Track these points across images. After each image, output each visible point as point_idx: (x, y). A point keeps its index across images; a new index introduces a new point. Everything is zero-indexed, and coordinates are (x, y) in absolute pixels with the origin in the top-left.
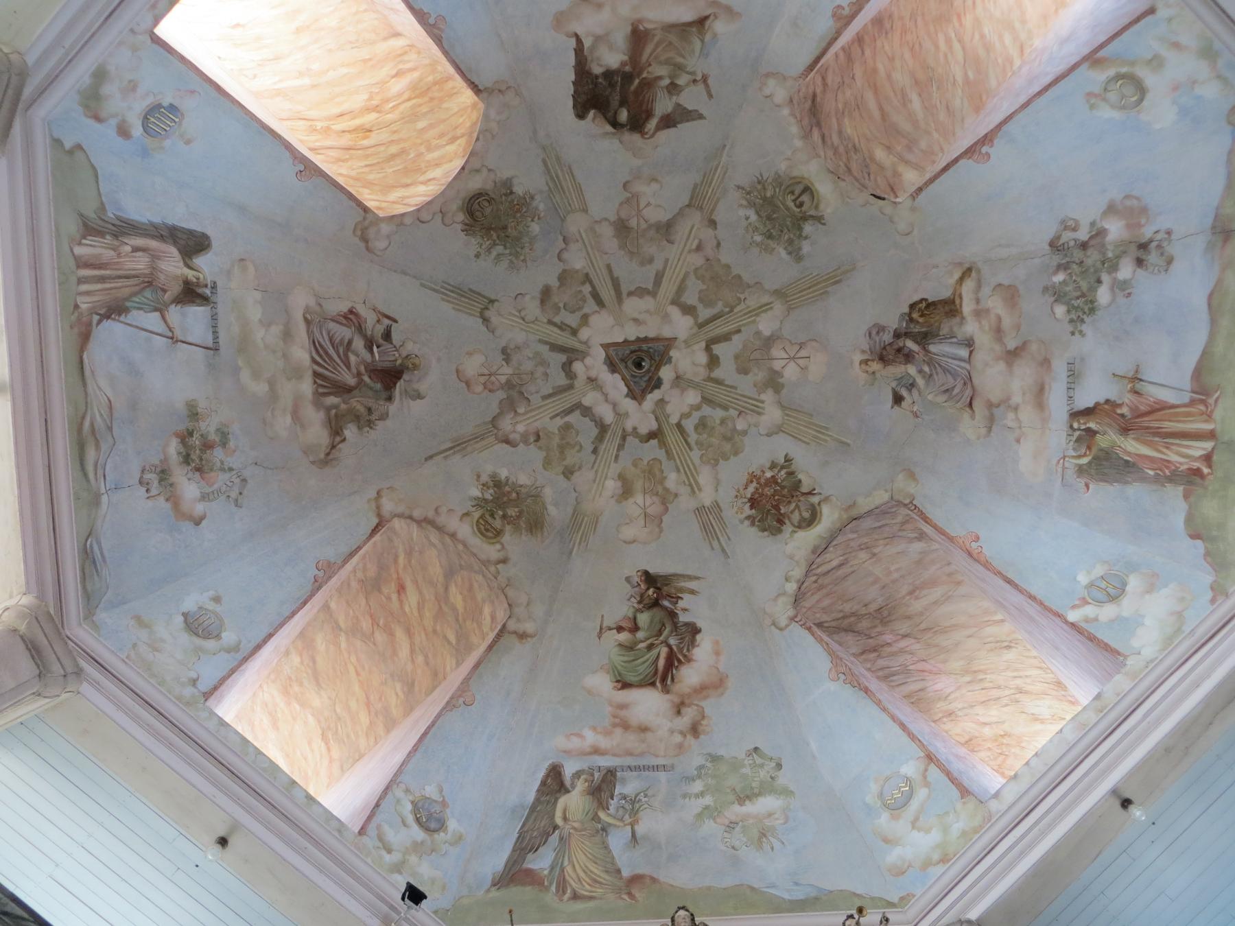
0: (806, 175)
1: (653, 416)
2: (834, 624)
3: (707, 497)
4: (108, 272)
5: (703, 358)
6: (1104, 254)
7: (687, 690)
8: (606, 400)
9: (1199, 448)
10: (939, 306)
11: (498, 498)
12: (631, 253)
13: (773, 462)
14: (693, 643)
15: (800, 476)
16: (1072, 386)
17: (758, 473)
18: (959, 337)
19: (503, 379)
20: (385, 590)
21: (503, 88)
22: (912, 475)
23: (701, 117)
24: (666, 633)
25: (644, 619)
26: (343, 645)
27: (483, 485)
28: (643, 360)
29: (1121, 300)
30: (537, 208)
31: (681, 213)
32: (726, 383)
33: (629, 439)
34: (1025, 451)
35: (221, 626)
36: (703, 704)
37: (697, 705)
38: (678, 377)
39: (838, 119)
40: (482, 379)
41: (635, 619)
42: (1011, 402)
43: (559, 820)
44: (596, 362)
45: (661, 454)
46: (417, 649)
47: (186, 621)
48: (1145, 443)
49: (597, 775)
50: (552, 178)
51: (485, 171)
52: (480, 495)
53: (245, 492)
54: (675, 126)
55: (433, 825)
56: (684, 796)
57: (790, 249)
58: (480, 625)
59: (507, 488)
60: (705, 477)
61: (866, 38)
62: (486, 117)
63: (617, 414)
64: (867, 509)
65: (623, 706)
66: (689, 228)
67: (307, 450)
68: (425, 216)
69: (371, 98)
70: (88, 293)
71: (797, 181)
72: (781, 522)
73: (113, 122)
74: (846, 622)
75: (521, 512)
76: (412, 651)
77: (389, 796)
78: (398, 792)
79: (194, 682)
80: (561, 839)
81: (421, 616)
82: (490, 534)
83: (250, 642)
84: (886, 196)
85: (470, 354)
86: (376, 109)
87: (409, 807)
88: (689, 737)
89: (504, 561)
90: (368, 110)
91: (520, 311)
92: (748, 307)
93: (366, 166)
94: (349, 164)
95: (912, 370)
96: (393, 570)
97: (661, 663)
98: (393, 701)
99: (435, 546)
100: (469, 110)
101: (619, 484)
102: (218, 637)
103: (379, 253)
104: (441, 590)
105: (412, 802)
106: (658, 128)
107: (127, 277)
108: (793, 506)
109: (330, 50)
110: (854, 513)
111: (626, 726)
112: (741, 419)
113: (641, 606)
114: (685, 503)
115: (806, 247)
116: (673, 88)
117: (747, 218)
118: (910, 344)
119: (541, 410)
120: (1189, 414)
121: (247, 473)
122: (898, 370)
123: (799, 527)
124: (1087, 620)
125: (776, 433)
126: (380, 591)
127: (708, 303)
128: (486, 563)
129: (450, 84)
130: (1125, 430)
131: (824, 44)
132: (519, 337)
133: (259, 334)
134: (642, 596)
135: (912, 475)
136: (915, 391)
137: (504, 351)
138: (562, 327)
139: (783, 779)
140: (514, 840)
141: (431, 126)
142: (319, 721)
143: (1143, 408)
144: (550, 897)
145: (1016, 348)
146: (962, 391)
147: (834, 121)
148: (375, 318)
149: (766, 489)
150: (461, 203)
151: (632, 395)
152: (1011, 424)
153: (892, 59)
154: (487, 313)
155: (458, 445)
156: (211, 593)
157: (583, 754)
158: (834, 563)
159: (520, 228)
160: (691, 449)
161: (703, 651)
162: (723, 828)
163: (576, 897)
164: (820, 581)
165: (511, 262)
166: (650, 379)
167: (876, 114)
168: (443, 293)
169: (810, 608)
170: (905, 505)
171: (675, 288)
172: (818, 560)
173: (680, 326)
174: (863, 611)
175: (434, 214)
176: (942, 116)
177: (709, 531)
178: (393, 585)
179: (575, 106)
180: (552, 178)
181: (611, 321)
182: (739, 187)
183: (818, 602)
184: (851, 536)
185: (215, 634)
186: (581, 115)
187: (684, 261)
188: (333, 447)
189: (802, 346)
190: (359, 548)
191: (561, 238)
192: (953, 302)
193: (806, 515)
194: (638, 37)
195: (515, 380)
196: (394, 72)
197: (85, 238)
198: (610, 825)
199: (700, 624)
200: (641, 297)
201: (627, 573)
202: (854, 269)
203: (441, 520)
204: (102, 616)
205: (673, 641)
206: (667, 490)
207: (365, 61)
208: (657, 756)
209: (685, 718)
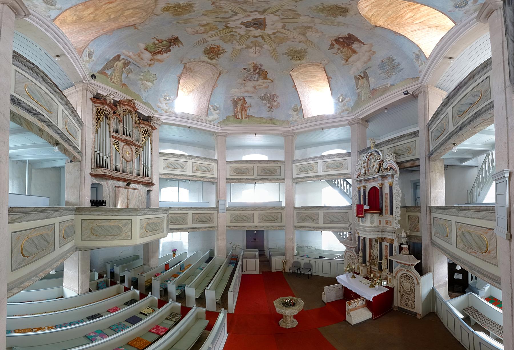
14: (166, 53)
15: (222, 55)
17: (220, 47)
22: (227, 72)
29: (263, 104)
34: (236, 90)
43: (115, 66)
48: (240, 109)
49: (127, 61)
56: (139, 74)
65: (142, 53)
72: (208, 54)
80: (114, 70)
95: (252, 71)
110: (216, 65)
111: (139, 56)
116: (339, 49)
118: (258, 71)
122: (252, 69)
123: (208, 57)
124: (210, 108)
130: (242, 105)
146: (247, 79)
152: (241, 87)
161: (165, 55)
163: (113, 82)
198: (124, 72)
205: (164, 50)
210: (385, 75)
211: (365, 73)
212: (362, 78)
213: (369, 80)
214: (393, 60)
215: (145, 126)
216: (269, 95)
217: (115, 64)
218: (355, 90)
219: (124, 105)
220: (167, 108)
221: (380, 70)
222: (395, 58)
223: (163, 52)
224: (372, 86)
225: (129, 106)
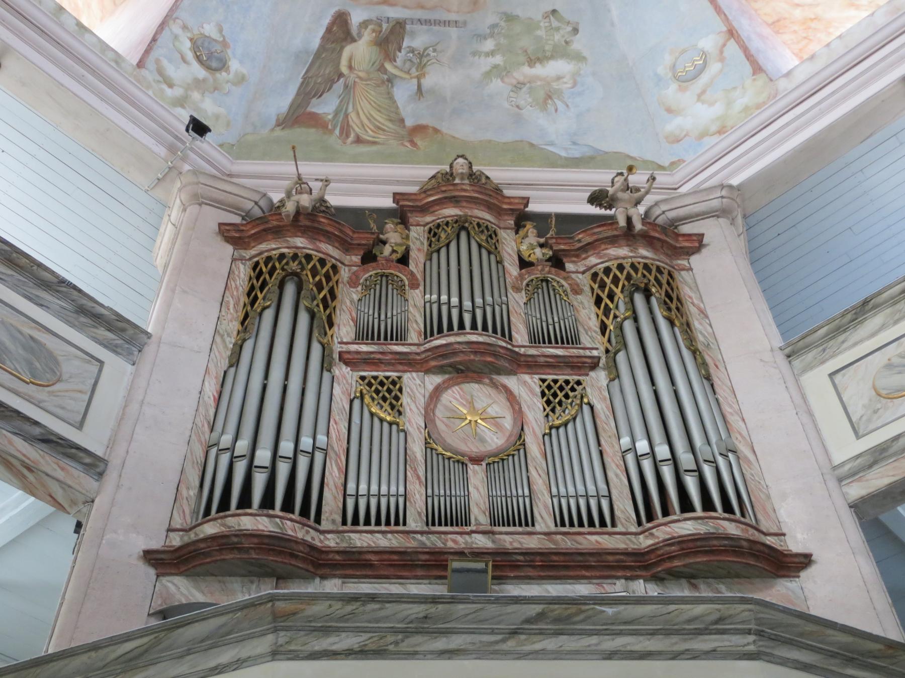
43: (344, 69)
49: (385, 26)
55: (214, 64)
56: (475, 53)
77: (166, 33)
78: (176, 28)
80: (346, 86)
87: (188, 44)
105: (191, 40)
139: (578, 44)
144: (334, 139)
163: (359, 140)
198: (396, 76)
208: (449, 11)
215: (598, 255)
219: (424, 209)
220: (718, 109)
225: (454, 200)
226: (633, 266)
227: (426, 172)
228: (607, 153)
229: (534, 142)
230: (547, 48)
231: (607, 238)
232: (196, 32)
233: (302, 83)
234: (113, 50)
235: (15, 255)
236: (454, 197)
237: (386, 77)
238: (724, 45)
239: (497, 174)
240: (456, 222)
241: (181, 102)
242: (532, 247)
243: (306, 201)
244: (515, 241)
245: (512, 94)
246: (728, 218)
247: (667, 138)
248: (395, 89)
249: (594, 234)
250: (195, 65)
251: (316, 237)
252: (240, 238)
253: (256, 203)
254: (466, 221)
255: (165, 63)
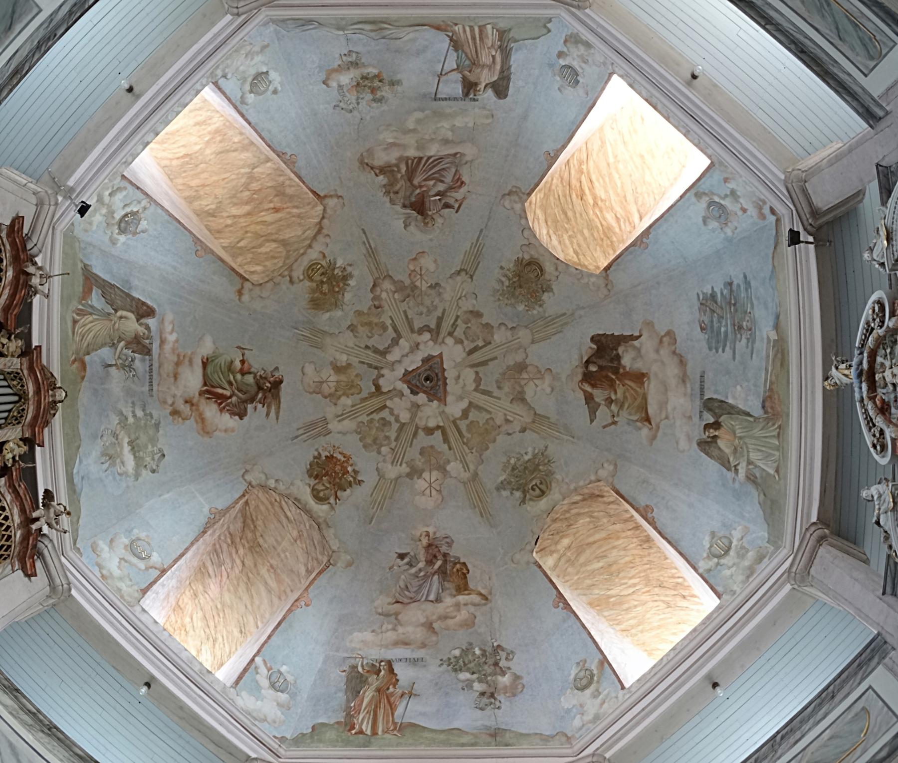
0: (552, 492)
1: (391, 389)
2: (248, 513)
3: (334, 426)
4: (478, 42)
5: (432, 424)
6: (490, 675)
7: (201, 408)
8: (403, 356)
9: (367, 728)
10: (463, 581)
11: (335, 278)
12: (504, 374)
13: (359, 472)
14: (233, 414)
15: (348, 491)
16: (408, 661)
17: (351, 462)
18: (443, 594)
19: (418, 284)
20: (276, 199)
21: (609, 287)
22: (349, 564)
23: (592, 421)
24: (240, 395)
25: (250, 379)
26: (243, 171)
27: (344, 268)
28: (431, 382)
29: (460, 685)
30: (534, 309)
31: (531, 408)
32: (415, 440)
33: (376, 372)
34: (368, 636)
35: (258, 93)
36: (192, 419)
37: (191, 415)
38: (418, 406)
39: (587, 512)
40: (418, 269)
41: (250, 373)
42: (399, 626)
43: (120, 313)
44: (430, 349)
45: (364, 394)
46: (236, 220)
47: (263, 73)
49: (147, 341)
50: (553, 319)
51: (557, 274)
52: (337, 266)
53: (343, 111)
54: (586, 403)
55: (123, 225)
56: (133, 403)
57: (505, 483)
58: (249, 263)
59: (341, 285)
60: (348, 425)
61: (638, 532)
62: (591, 275)
63: (393, 364)
64: (326, 535)
66: (520, 413)
67: (370, 151)
68: (526, 233)
69: (602, 200)
70: (465, 31)
71: (549, 487)
72: (316, 477)
73: (565, 50)
74: (250, 522)
75: (325, 294)
76: (234, 216)
77: (142, 196)
78: (144, 203)
79: (225, 76)
80: (109, 314)
81: (257, 223)
82: (310, 271)
83: (247, 111)
84: (537, 546)
85: (435, 261)
86: (595, 204)
87: (135, 210)
88: (171, 408)
89: (291, 281)
90: (595, 198)
91: (465, 296)
92: (467, 455)
93: (559, 196)
94: (560, 185)
95: (421, 565)
96: (289, 205)
97: (220, 391)
98: (204, 203)
99: (303, 233)
100: (595, 264)
101: (344, 364)
102: (251, 92)
103: (502, 202)
104: (274, 237)
105: (138, 211)
106: (585, 392)
107: (476, 52)
108: (328, 485)
109: (631, 176)
110: (323, 526)
111: (178, 364)
112: (389, 450)
113: (258, 377)
114: (331, 411)
115: (505, 493)
116: (609, 401)
117: (526, 453)
118: (439, 563)
119: (397, 310)
120: (388, 722)
121: (355, 113)
122: (422, 556)
123: (313, 489)
124: (256, 668)
125: (379, 475)
126: (276, 195)
127: (469, 427)
128: (290, 268)
129: (611, 252)
130: (378, 690)
131: (631, 500)
132: (447, 296)
133: (446, 124)
134: (266, 378)
135: (349, 564)
136: (407, 567)
137: (437, 284)
138: (455, 326)
139: (145, 473)
140: (110, 281)
141: (585, 239)
142: (196, 153)
143: (392, 699)
144: (75, 305)
145: (434, 628)
146: (406, 597)
147: (587, 510)
148: (458, 199)
149: (339, 467)
150: (536, 257)
151: (407, 373)
152: (384, 627)
153: (625, 549)
154: (463, 273)
155: (373, 252)
156: (280, 88)
157: (161, 333)
158: (289, 514)
159: (521, 297)
160: (368, 415)
161: (227, 420)
162: (114, 430)
163: (75, 322)
164: (276, 503)
165: (498, 291)
166: (417, 387)
167: (591, 540)
168: (476, 245)
169: (257, 496)
170: (329, 561)
171: (481, 405)
172: (291, 502)
173: (455, 408)
174: (258, 534)
175: (528, 239)
176: (588, 582)
177: (311, 426)
178: (279, 205)
179: (599, 335)
180: (553, 319)
181: (459, 360)
182: (546, 447)
183: (262, 502)
184: (307, 525)
185: (254, 90)
186: (593, 339)
187: (499, 411)
188: (372, 168)
189: (439, 491)
190: (304, 182)
191: (514, 325)
192: (466, 590)
193: (321, 494)
194: (640, 377)
195: (417, 292)
196: (619, 216)
197: (497, 30)
198: (116, 349)
199: (246, 419)
200: (475, 381)
201: (281, 368)
202: (491, 526)
203: (321, 238)
204: (272, 27)
205: (234, 399)
206: (339, 398)
207: (625, 197)
208: (158, 385)
209: (182, 406)
210: (744, 341)
211: (709, 405)
212: (716, 425)
213: (732, 407)
214: (713, 296)
215: (12, 501)
216: (477, 652)
217: (124, 313)
218: (734, 480)
219: (31, 369)
220: (117, 572)
221: (723, 351)
222: (709, 287)
223: (228, 405)
224: (754, 406)
225: (38, 392)
226: (8, 527)
227: (56, 372)
228: (79, 502)
229: (80, 449)
230: (141, 453)
231: (24, 505)
232: (142, 215)
233: (111, 284)
234: (133, 161)
235: (19, 76)
236: (40, 391)
237: (115, 342)
238: (156, 568)
239: (57, 420)
240: (24, 393)
241: (100, 200)
242: (12, 451)
243: (35, 281)
244: (15, 438)
245: (110, 431)
246: (50, 593)
247: (94, 543)
248: (108, 348)
249: (25, 496)
250: (123, 213)
251: (13, 287)
252: (14, 230)
253: (36, 245)
254: (25, 400)
255: (124, 193)
